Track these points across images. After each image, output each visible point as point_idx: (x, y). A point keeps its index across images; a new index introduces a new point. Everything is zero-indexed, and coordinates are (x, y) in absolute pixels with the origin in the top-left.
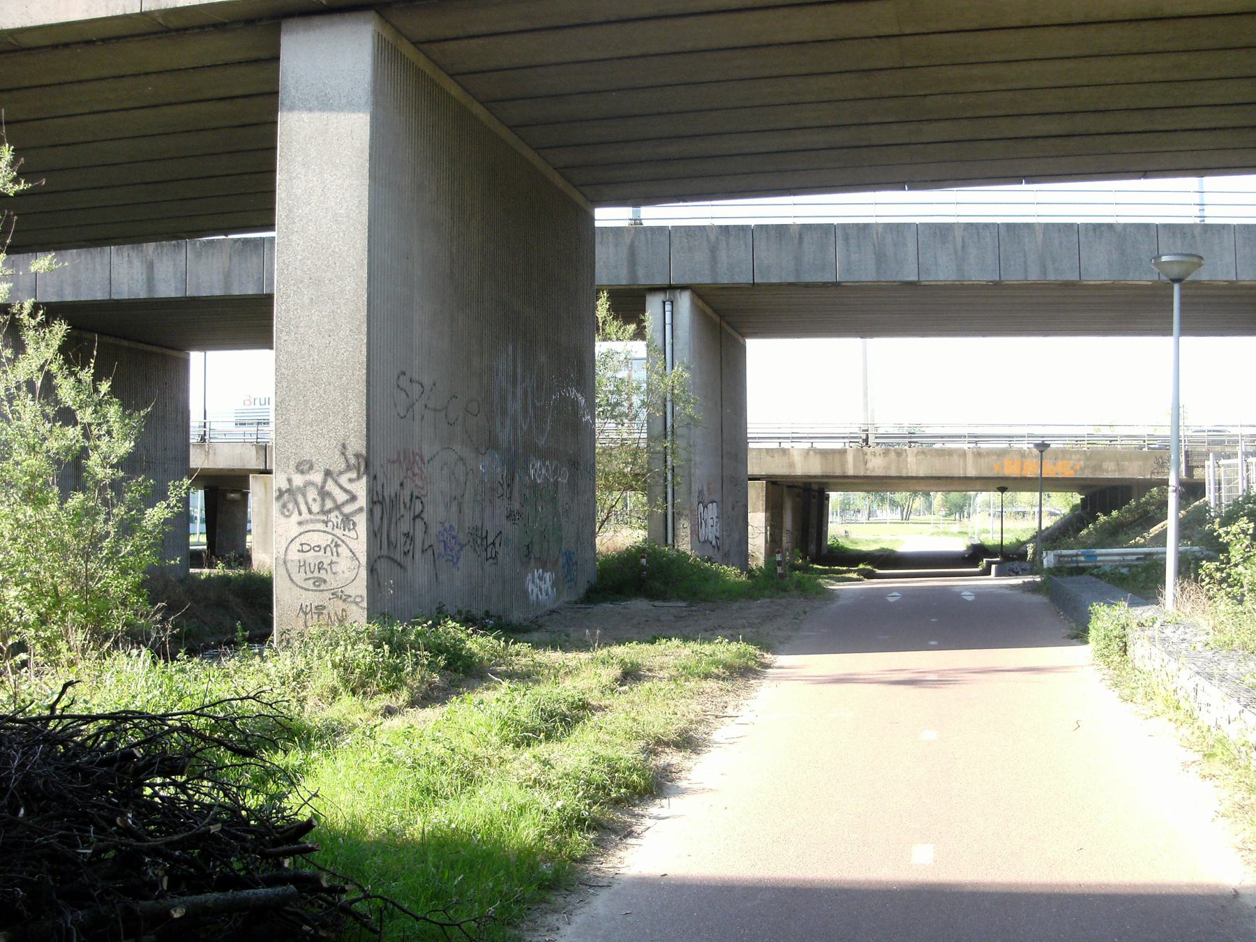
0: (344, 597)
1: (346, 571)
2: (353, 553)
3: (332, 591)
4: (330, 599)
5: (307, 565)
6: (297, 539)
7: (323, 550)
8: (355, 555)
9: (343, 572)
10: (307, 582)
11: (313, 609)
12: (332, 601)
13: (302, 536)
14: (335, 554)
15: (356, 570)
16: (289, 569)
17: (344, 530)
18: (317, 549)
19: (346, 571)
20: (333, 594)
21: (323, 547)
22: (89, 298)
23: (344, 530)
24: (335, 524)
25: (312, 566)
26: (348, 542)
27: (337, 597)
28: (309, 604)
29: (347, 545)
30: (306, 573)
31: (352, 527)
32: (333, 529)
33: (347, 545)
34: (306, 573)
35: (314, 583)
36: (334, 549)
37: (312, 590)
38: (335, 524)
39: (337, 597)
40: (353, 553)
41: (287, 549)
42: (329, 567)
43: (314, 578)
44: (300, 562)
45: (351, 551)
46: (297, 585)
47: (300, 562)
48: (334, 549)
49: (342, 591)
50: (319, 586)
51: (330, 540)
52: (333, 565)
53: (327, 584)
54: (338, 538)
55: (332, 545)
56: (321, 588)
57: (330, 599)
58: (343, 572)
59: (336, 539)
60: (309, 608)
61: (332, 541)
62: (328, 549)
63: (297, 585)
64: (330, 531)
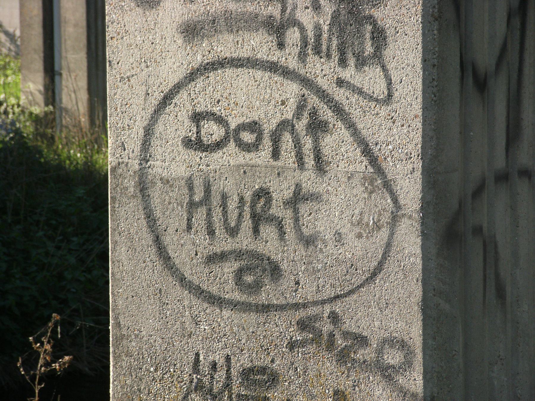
0: (340, 342)
1: (350, 237)
2: (373, 161)
3: (301, 314)
4: (292, 346)
5: (216, 200)
6: (182, 97)
7: (267, 143)
8: (380, 171)
9: (242, 107)
10: (216, 268)
11: (236, 382)
12: (299, 354)
13: (200, 83)
14: (310, 162)
15: (384, 233)
16: (158, 213)
17: (343, 62)
18: (248, 137)
19: (350, 237)
20: (303, 325)
21: (269, 127)
22: (418, 124)
23: (343, 62)
24: (310, 34)
25: (233, 204)
26: (355, 114)
27: (317, 338)
28: (221, 362)
29: (351, 126)
30: (211, 232)
31: (369, 49)
32: (302, 56)
33: (351, 126)
34: (211, 232)
35: (239, 274)
36: (308, 143)
37: (234, 305)
38: (310, 34)
39: (317, 338)
40: (373, 161)
41: (148, 132)
42: (287, 215)
43: (238, 254)
44: (191, 188)
45: (367, 151)
46: (182, 280)
47: (191, 188)
48: (308, 143)
49: (334, 318)
50: (256, 287)
51: (292, 104)
52: (304, 208)
53: (287, 283)
54: (323, 95)
55: (301, 125)
56: (263, 298)
57: (292, 346)
58: (339, 237)
59: (313, 100)
60: (221, 375)
61: (300, 108)
62: (287, 138)
63: (182, 280)
64: (293, 63)
